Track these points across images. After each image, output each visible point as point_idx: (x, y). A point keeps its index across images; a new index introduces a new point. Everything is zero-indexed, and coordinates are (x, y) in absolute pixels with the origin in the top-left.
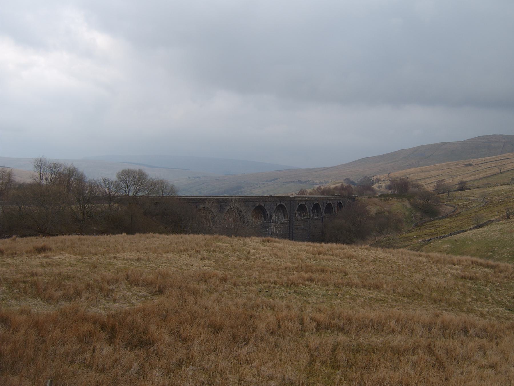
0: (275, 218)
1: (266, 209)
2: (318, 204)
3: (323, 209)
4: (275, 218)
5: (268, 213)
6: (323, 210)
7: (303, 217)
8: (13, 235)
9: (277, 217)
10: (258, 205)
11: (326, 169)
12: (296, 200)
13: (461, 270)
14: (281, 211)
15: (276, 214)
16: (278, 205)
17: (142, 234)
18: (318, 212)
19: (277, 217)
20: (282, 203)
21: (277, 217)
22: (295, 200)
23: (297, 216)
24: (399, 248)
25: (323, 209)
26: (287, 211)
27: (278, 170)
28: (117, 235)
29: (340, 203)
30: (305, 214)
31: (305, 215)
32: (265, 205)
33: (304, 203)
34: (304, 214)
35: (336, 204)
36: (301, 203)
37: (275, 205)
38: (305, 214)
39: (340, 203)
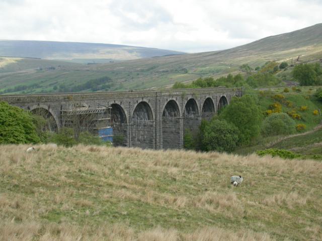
0: (137, 119)
2: (173, 100)
3: (182, 108)
4: (137, 119)
5: (126, 112)
6: (200, 108)
11: (234, 52)
12: (164, 96)
14: (145, 110)
16: (139, 102)
18: (194, 110)
20: (145, 100)
24: (127, 183)
25: (182, 108)
26: (152, 109)
28: (189, 151)
29: (223, 97)
32: (121, 103)
33: (174, 99)
35: (219, 99)
36: (171, 99)
37: (135, 103)
39: (223, 97)
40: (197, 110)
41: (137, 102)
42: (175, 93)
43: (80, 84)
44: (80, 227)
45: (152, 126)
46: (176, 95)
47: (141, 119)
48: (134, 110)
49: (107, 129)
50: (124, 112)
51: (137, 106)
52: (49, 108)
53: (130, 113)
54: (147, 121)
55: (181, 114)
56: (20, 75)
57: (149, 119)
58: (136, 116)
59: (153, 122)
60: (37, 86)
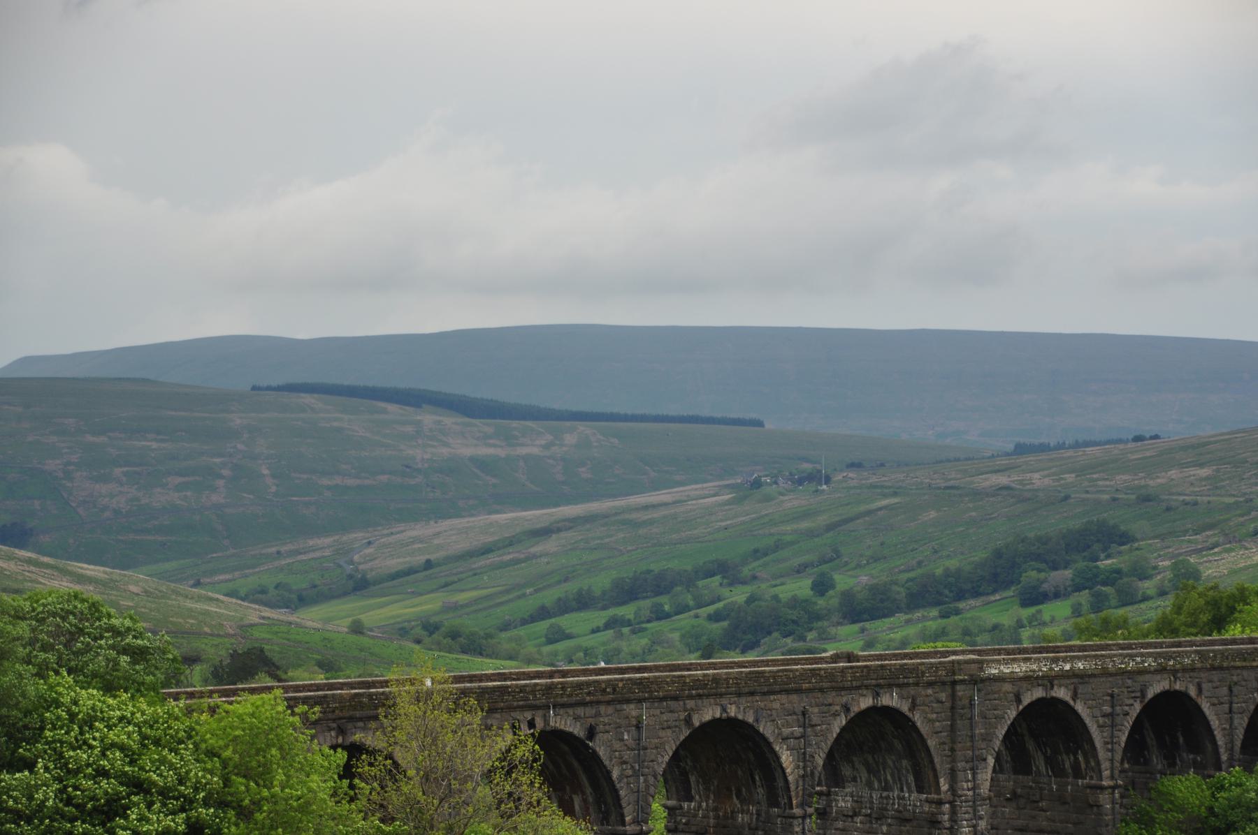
1: (771, 740)
2: (1183, 696)
5: (786, 758)
7: (1070, 780)
8: (225, 759)
9: (880, 782)
10: (707, 717)
13: (240, 764)
14: (898, 745)
15: (870, 759)
17: (432, 522)
19: (876, 785)
21: (876, 785)
22: (983, 681)
23: (1039, 773)
27: (1021, 449)
30: (1081, 758)
31: (1083, 766)
34: (1076, 759)
36: (1039, 693)
37: (836, 715)
38: (1081, 758)
40: (1209, 747)
41: (1018, 700)
42: (1067, 667)
43: (953, 564)
44: (198, 727)
45: (934, 823)
46: (1074, 675)
47: (887, 788)
48: (826, 747)
49: (671, 825)
50: (778, 758)
51: (843, 730)
52: (913, 707)
53: (804, 758)
54: (915, 800)
55: (1105, 765)
56: (634, 516)
57: (920, 790)
58: (864, 775)
59: (940, 803)
60: (726, 571)
